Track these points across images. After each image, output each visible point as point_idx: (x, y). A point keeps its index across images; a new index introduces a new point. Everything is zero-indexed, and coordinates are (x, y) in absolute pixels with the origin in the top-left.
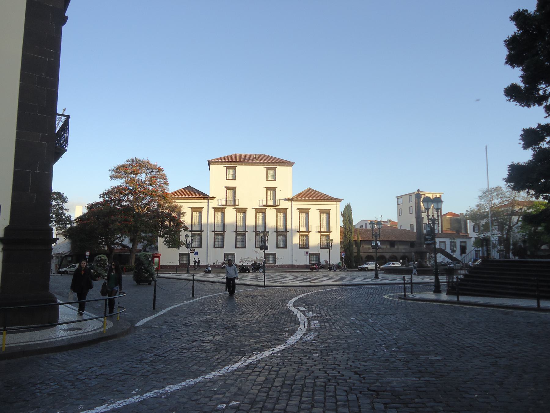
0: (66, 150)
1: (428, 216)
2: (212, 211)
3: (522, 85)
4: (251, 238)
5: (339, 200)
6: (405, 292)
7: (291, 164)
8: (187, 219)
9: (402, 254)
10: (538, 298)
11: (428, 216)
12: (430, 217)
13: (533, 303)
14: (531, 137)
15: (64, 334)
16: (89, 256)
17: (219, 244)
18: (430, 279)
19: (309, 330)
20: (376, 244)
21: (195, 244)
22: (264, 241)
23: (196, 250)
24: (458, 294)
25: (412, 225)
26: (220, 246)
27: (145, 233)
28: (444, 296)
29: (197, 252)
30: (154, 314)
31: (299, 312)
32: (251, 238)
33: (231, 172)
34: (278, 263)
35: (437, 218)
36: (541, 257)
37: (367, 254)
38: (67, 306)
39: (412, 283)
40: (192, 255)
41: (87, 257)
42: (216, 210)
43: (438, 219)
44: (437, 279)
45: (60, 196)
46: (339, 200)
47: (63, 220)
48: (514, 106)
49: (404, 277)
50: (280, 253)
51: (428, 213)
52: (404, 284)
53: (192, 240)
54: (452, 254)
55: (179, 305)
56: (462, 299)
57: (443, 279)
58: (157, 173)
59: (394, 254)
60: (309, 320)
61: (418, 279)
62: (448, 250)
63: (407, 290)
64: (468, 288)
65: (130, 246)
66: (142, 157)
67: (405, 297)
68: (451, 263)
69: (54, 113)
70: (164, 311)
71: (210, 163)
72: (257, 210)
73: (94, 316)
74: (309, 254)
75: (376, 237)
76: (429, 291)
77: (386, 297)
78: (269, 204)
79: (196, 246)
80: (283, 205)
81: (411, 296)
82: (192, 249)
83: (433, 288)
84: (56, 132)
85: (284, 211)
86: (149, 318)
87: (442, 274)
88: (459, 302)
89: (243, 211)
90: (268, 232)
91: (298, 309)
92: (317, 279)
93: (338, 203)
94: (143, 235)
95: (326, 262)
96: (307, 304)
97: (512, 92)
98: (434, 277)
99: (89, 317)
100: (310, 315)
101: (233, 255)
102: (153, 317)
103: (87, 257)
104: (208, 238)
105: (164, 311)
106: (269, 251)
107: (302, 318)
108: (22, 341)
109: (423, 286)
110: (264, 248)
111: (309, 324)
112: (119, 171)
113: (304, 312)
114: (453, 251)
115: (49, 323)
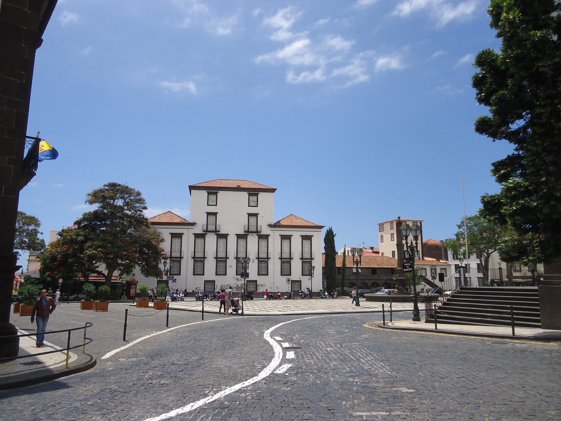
0: (35, 174)
1: (407, 243)
2: (193, 237)
3: (517, 145)
4: (232, 263)
5: (321, 227)
6: (384, 320)
7: (273, 190)
8: (165, 246)
9: (384, 281)
10: (513, 325)
11: (407, 243)
12: (409, 245)
13: (507, 330)
14: (502, 169)
15: (23, 368)
16: (62, 283)
17: (199, 271)
18: (410, 306)
19: (284, 360)
20: (357, 271)
21: (175, 271)
22: (246, 268)
23: (175, 277)
24: (436, 322)
25: (393, 252)
26: (199, 273)
27: (122, 260)
28: (422, 325)
29: (175, 280)
30: (125, 345)
31: (275, 342)
32: (232, 263)
33: (213, 197)
34: (261, 290)
35: (415, 245)
36: (518, 284)
37: (373, 281)
38: (31, 338)
39: (391, 311)
40: (170, 282)
41: (60, 285)
42: (197, 236)
43: (417, 247)
44: (416, 307)
45: (33, 220)
46: (321, 227)
47: (34, 245)
48: (485, 139)
49: (383, 305)
50: (261, 280)
51: (407, 241)
52: (384, 311)
53: (170, 267)
54: (432, 281)
55: (152, 335)
56: (440, 327)
57: (422, 306)
58: (135, 199)
59: (376, 281)
60: (285, 350)
61: (397, 306)
62: (429, 277)
63: (386, 318)
64: (447, 316)
65: (106, 273)
66: (121, 181)
67: (384, 326)
68: (69, 248)
69: (22, 136)
70: (135, 342)
71: (191, 188)
72: (239, 236)
73: (59, 348)
74: (290, 282)
75: (357, 265)
76: (406, 318)
77: (366, 326)
78: (250, 230)
79: (175, 273)
80: (265, 231)
81: (390, 324)
82: (171, 277)
83: (413, 316)
84: (25, 156)
85: (266, 237)
86: (117, 350)
87: (422, 302)
88: (436, 331)
89: (225, 236)
90: (249, 258)
91: (275, 339)
92: (297, 307)
93: (319, 230)
94: (120, 261)
95: (308, 289)
96: (285, 335)
97: (483, 126)
98: (413, 304)
99: (53, 350)
100: (286, 345)
101: (213, 282)
102: (122, 348)
103: (60, 285)
104: (187, 265)
105: (135, 342)
106: (250, 278)
107: (278, 350)
108: (10, 372)
109: (402, 315)
110: (245, 275)
111: (284, 355)
112: (96, 196)
113: (279, 342)
114: (434, 278)
115: (8, 356)
